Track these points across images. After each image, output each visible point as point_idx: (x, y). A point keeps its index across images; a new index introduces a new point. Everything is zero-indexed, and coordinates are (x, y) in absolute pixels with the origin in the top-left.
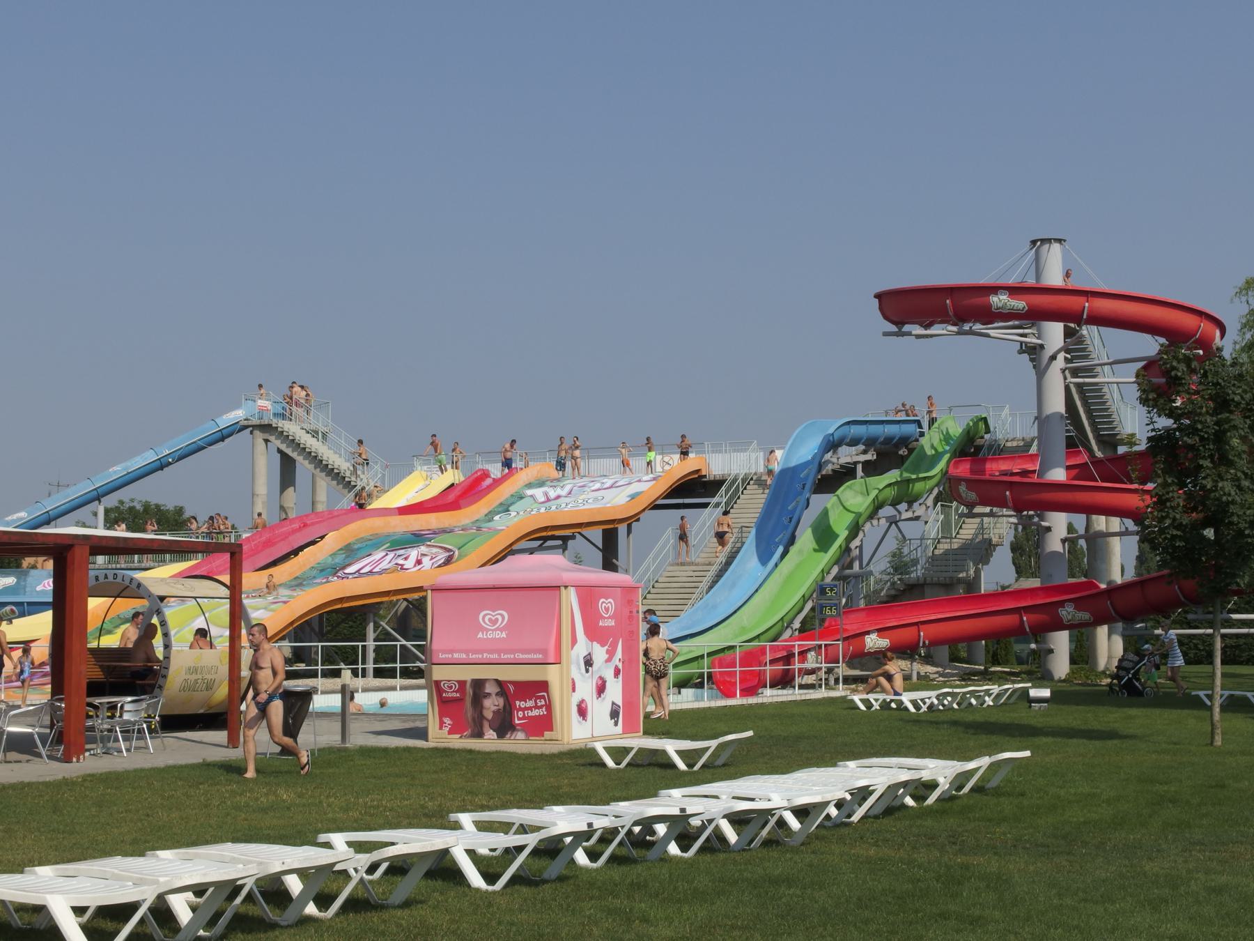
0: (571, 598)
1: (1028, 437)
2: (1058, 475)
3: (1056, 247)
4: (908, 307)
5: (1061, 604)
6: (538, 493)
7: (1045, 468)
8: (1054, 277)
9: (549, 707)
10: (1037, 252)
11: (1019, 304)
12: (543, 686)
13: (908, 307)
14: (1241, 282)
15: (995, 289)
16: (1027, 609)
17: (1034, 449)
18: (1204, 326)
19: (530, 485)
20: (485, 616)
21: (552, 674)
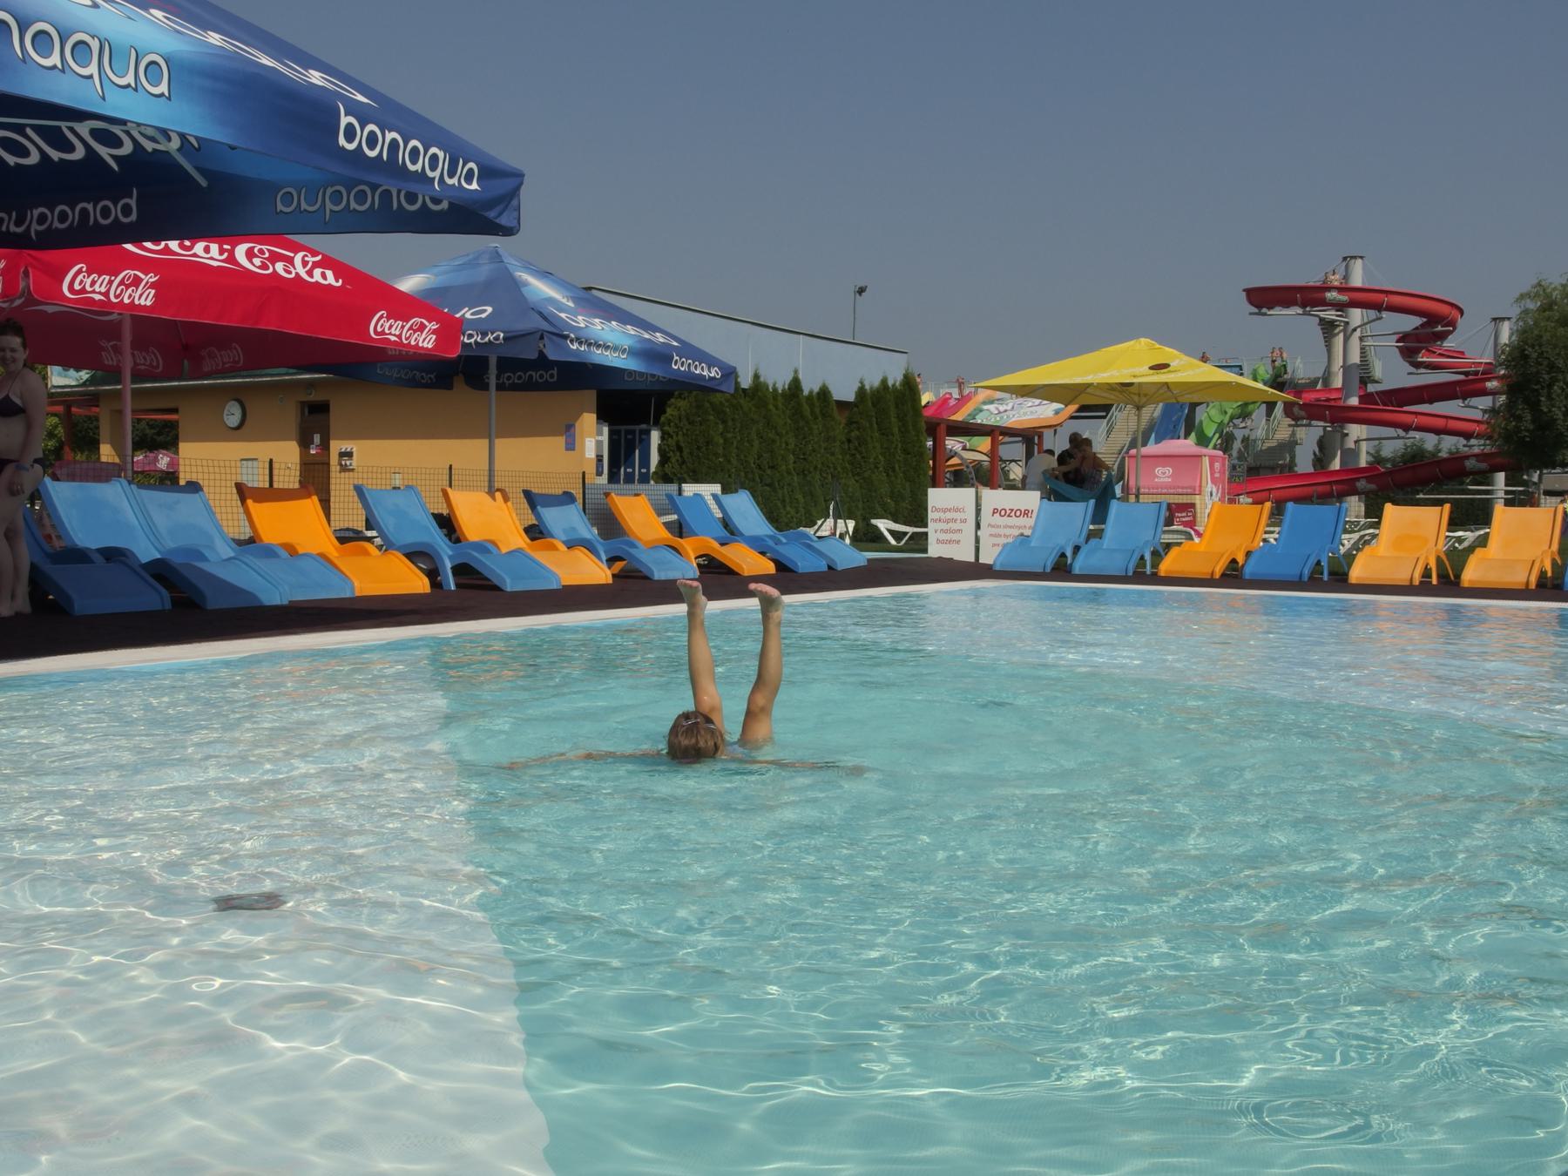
0: (1206, 461)
1: (1313, 376)
2: (1354, 401)
3: (1359, 261)
4: (1263, 298)
5: (1358, 479)
6: (991, 407)
7: (1348, 396)
8: (1357, 280)
9: (1194, 517)
10: (1347, 267)
11: (1344, 298)
12: (1193, 505)
13: (1263, 298)
14: (1517, 295)
15: (1329, 289)
16: (1336, 482)
17: (1319, 386)
18: (1454, 312)
19: (985, 403)
20: (1159, 470)
21: (1197, 500)
